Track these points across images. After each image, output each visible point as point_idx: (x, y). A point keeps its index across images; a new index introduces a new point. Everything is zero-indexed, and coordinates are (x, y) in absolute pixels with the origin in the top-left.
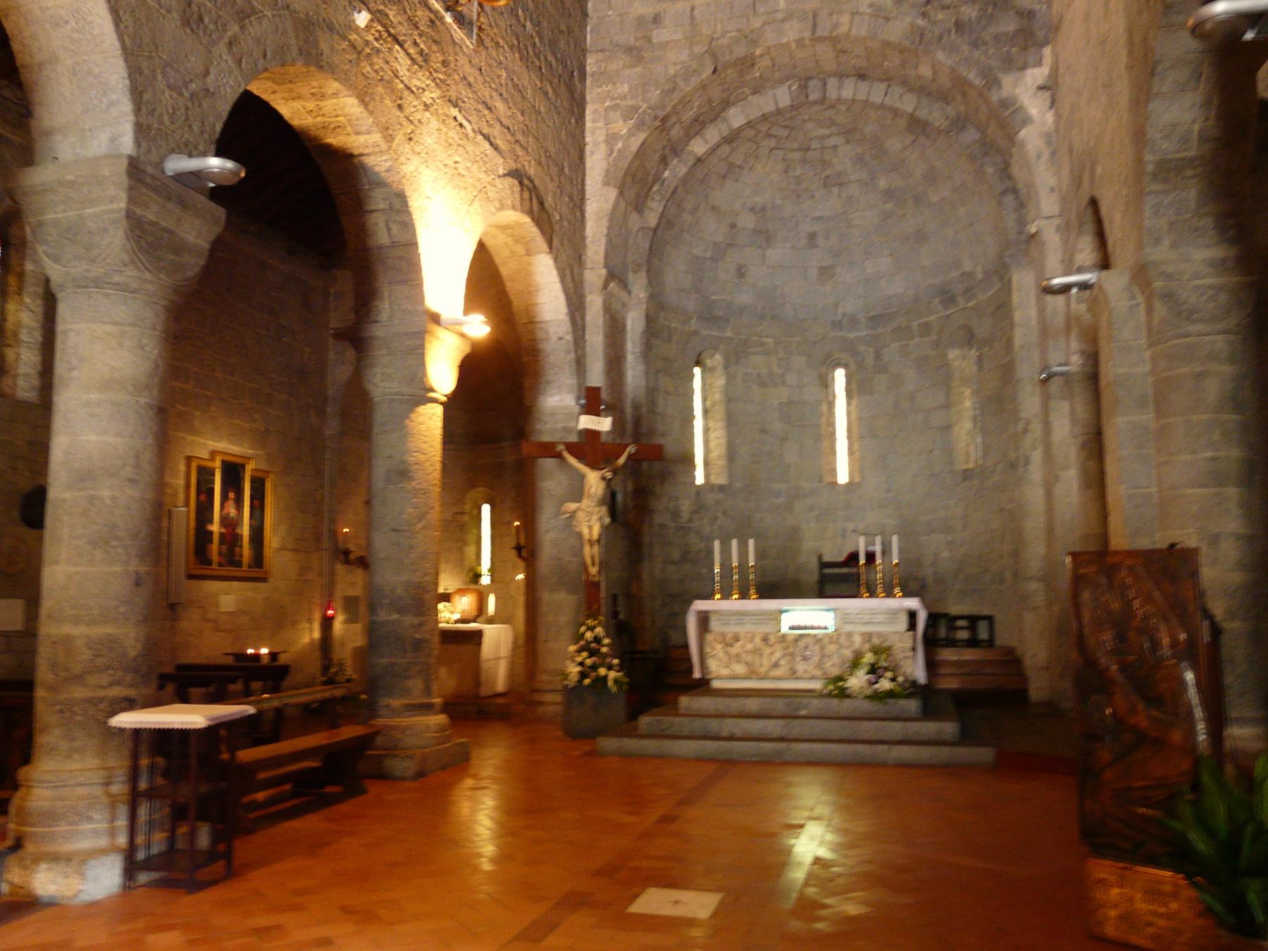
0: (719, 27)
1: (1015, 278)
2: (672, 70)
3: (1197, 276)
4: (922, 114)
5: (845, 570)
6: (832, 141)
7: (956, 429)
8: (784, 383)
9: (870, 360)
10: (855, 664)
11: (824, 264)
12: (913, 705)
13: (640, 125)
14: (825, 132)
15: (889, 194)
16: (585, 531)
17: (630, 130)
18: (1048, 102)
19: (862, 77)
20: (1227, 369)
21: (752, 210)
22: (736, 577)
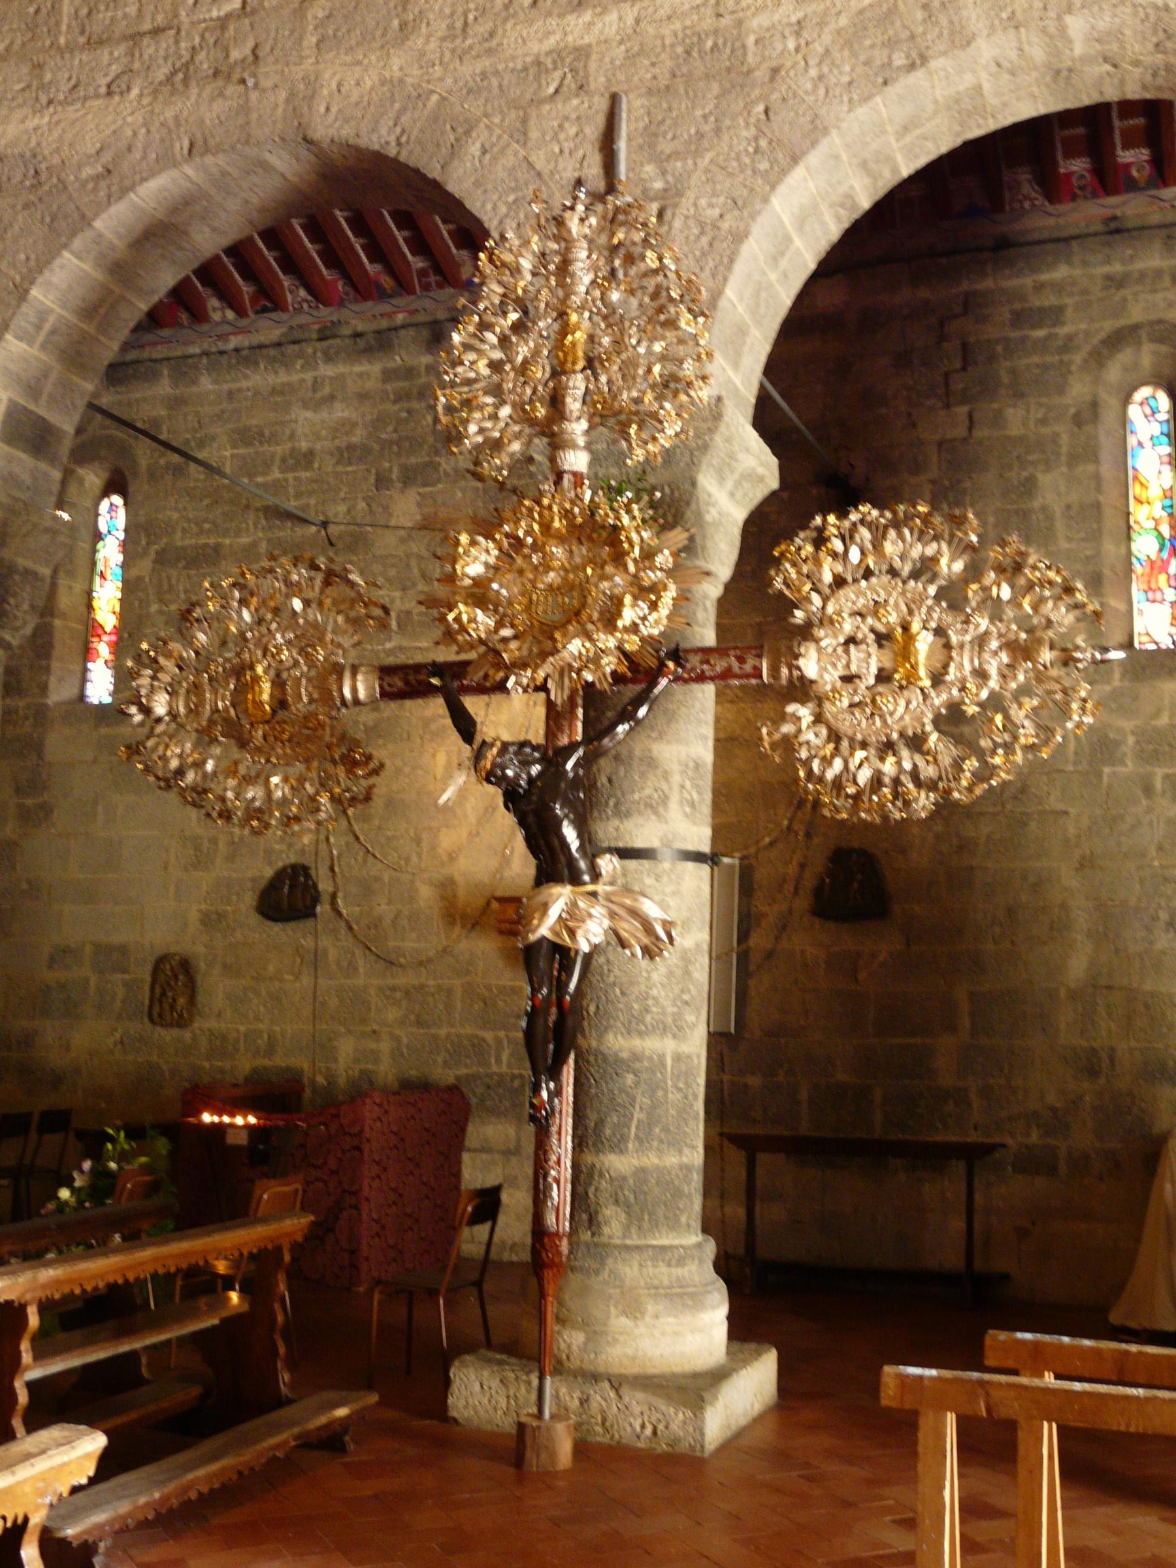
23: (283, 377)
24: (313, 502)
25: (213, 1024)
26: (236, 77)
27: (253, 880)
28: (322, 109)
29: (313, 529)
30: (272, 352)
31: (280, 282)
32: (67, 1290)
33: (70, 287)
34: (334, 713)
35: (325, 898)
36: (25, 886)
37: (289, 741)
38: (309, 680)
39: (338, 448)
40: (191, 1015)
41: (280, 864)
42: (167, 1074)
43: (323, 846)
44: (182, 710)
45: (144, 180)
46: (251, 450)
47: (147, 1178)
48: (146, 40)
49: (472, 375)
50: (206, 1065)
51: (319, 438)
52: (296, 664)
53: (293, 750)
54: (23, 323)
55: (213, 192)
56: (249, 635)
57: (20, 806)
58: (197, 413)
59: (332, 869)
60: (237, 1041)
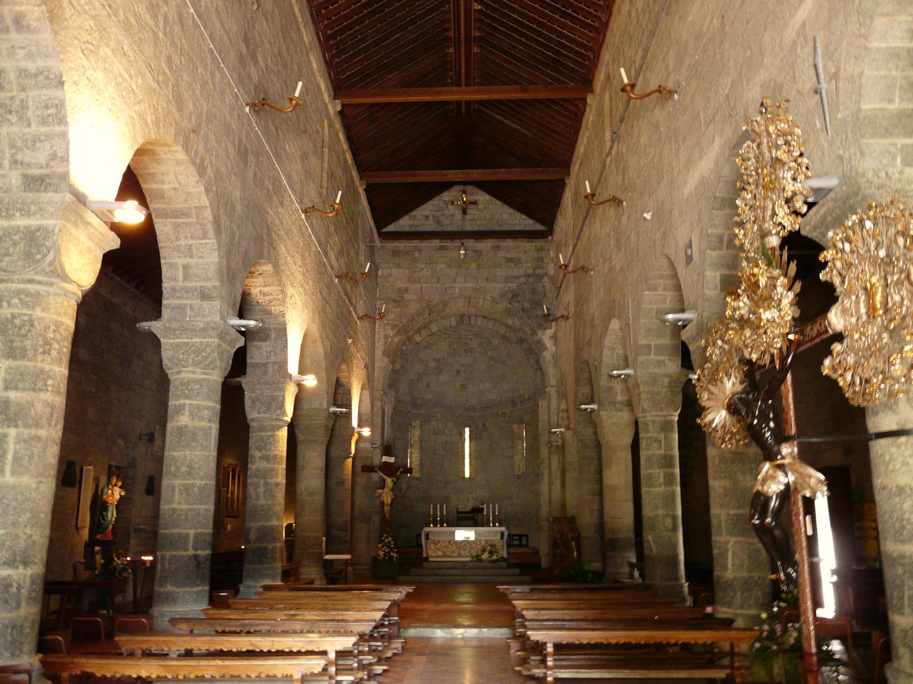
1: (540, 403)
5: (468, 515)
6: (471, 337)
10: (484, 550)
13: (399, 333)
15: (491, 358)
16: (385, 500)
19: (485, 317)
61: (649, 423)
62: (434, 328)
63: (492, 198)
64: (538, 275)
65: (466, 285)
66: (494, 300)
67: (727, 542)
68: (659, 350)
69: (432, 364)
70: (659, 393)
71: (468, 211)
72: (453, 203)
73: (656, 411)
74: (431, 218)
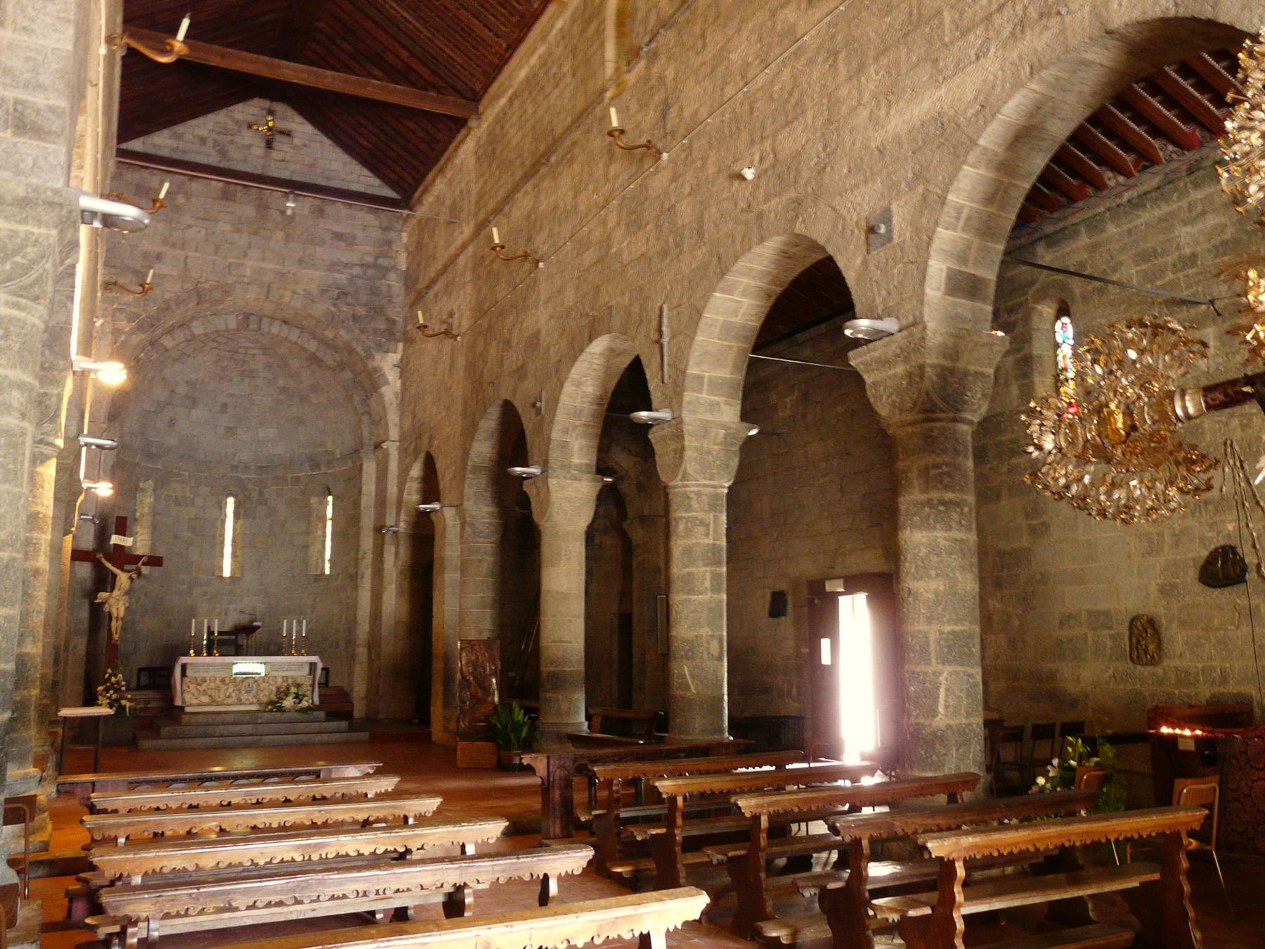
0: (204, 275)
2: (167, 295)
3: (483, 518)
4: (320, 354)
6: (255, 351)
7: (311, 549)
8: (193, 505)
9: (255, 495)
11: (231, 425)
12: (321, 714)
13: (140, 328)
14: (251, 345)
15: (283, 390)
16: (114, 611)
17: (131, 329)
18: (398, 374)
19: (285, 322)
20: (490, 559)
21: (187, 382)
22: (205, 642)
23: (1165, 209)
24: (1200, 289)
25: (1177, 662)
26: (1054, 12)
27: (1194, 560)
28: (1116, 6)
29: (1204, 307)
30: (1154, 194)
31: (1152, 146)
32: (986, 852)
33: (974, 188)
34: (1172, 428)
35: (1252, 568)
36: (1038, 576)
37: (1141, 454)
38: (1150, 407)
39: (1215, 247)
40: (1160, 657)
41: (1213, 547)
42: (1149, 699)
43: (1245, 531)
44: (1064, 444)
45: (1005, 103)
46: (1150, 264)
47: (1099, 773)
48: (994, 17)
49: (1247, 148)
50: (1177, 692)
51: (1198, 243)
52: (1139, 398)
53: (1145, 460)
54: (947, 219)
55: (1054, 94)
56: (1102, 383)
57: (1029, 526)
58: (1108, 250)
59: (1254, 546)
60: (1197, 674)
61: (692, 496)
62: (198, 328)
63: (316, 132)
64: (382, 267)
65: (264, 265)
66: (308, 295)
67: (937, 674)
68: (715, 386)
69: (182, 389)
70: (709, 452)
71: (275, 145)
72: (250, 127)
73: (705, 479)
74: (210, 143)
